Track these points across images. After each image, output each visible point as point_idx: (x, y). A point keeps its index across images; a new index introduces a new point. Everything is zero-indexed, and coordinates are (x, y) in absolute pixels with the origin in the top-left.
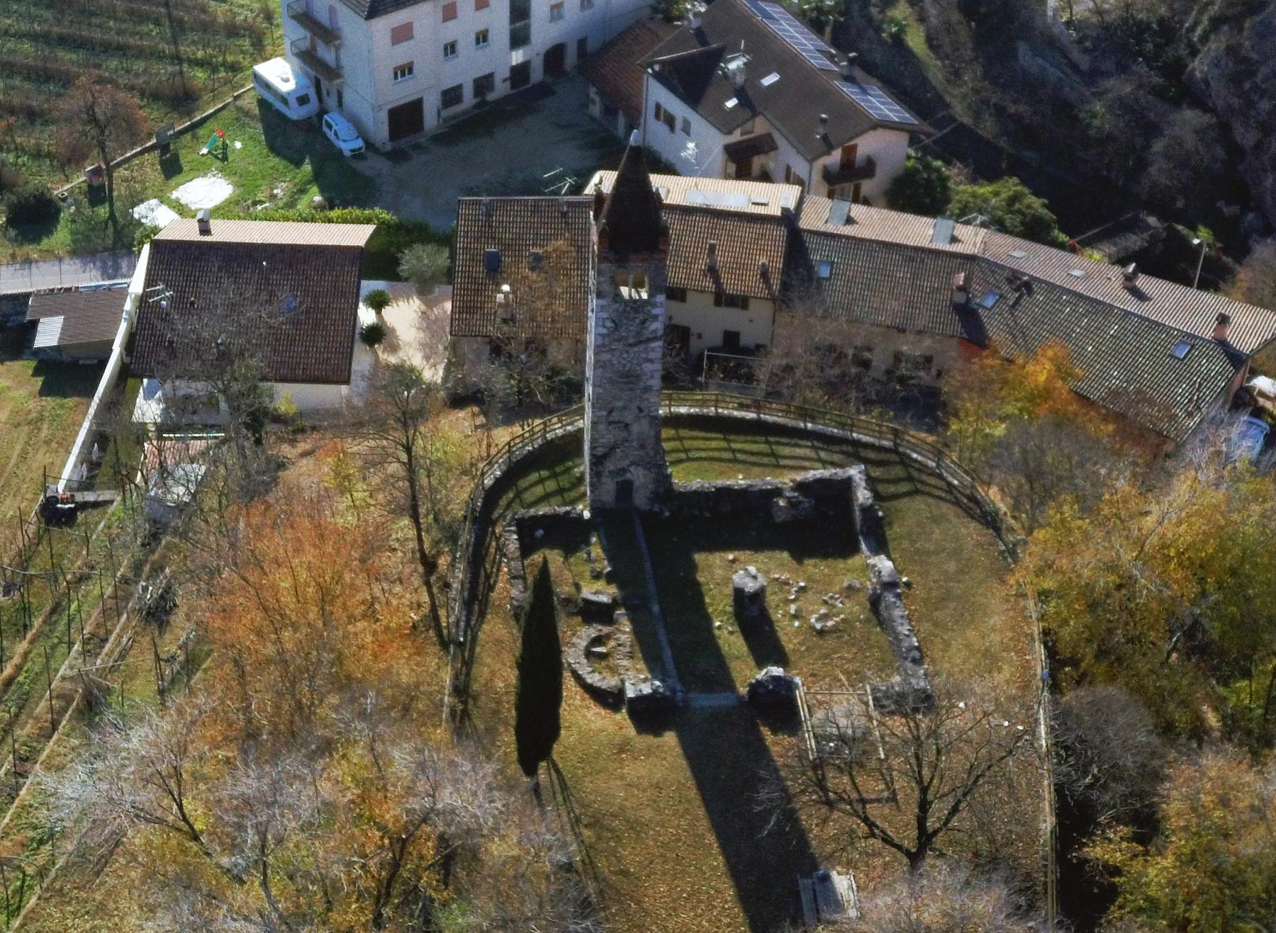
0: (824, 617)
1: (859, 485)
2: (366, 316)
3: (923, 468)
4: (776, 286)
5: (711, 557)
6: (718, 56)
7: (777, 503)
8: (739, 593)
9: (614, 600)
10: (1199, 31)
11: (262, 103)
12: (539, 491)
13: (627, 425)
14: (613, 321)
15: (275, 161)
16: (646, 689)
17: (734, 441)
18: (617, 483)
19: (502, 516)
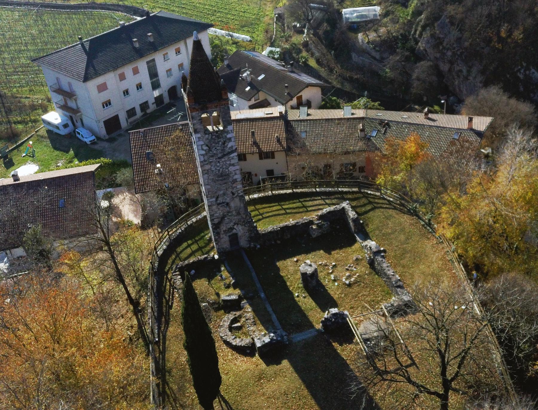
0: (349, 277)
1: (349, 210)
2: (105, 204)
3: (375, 197)
4: (285, 145)
5: (285, 262)
6: (239, 72)
7: (312, 227)
8: (304, 275)
9: (239, 296)
10: (418, 32)
11: (49, 131)
12: (189, 251)
13: (228, 204)
14: (207, 146)
15: (57, 153)
16: (267, 340)
17: (284, 205)
18: (229, 236)
19: (171, 268)
